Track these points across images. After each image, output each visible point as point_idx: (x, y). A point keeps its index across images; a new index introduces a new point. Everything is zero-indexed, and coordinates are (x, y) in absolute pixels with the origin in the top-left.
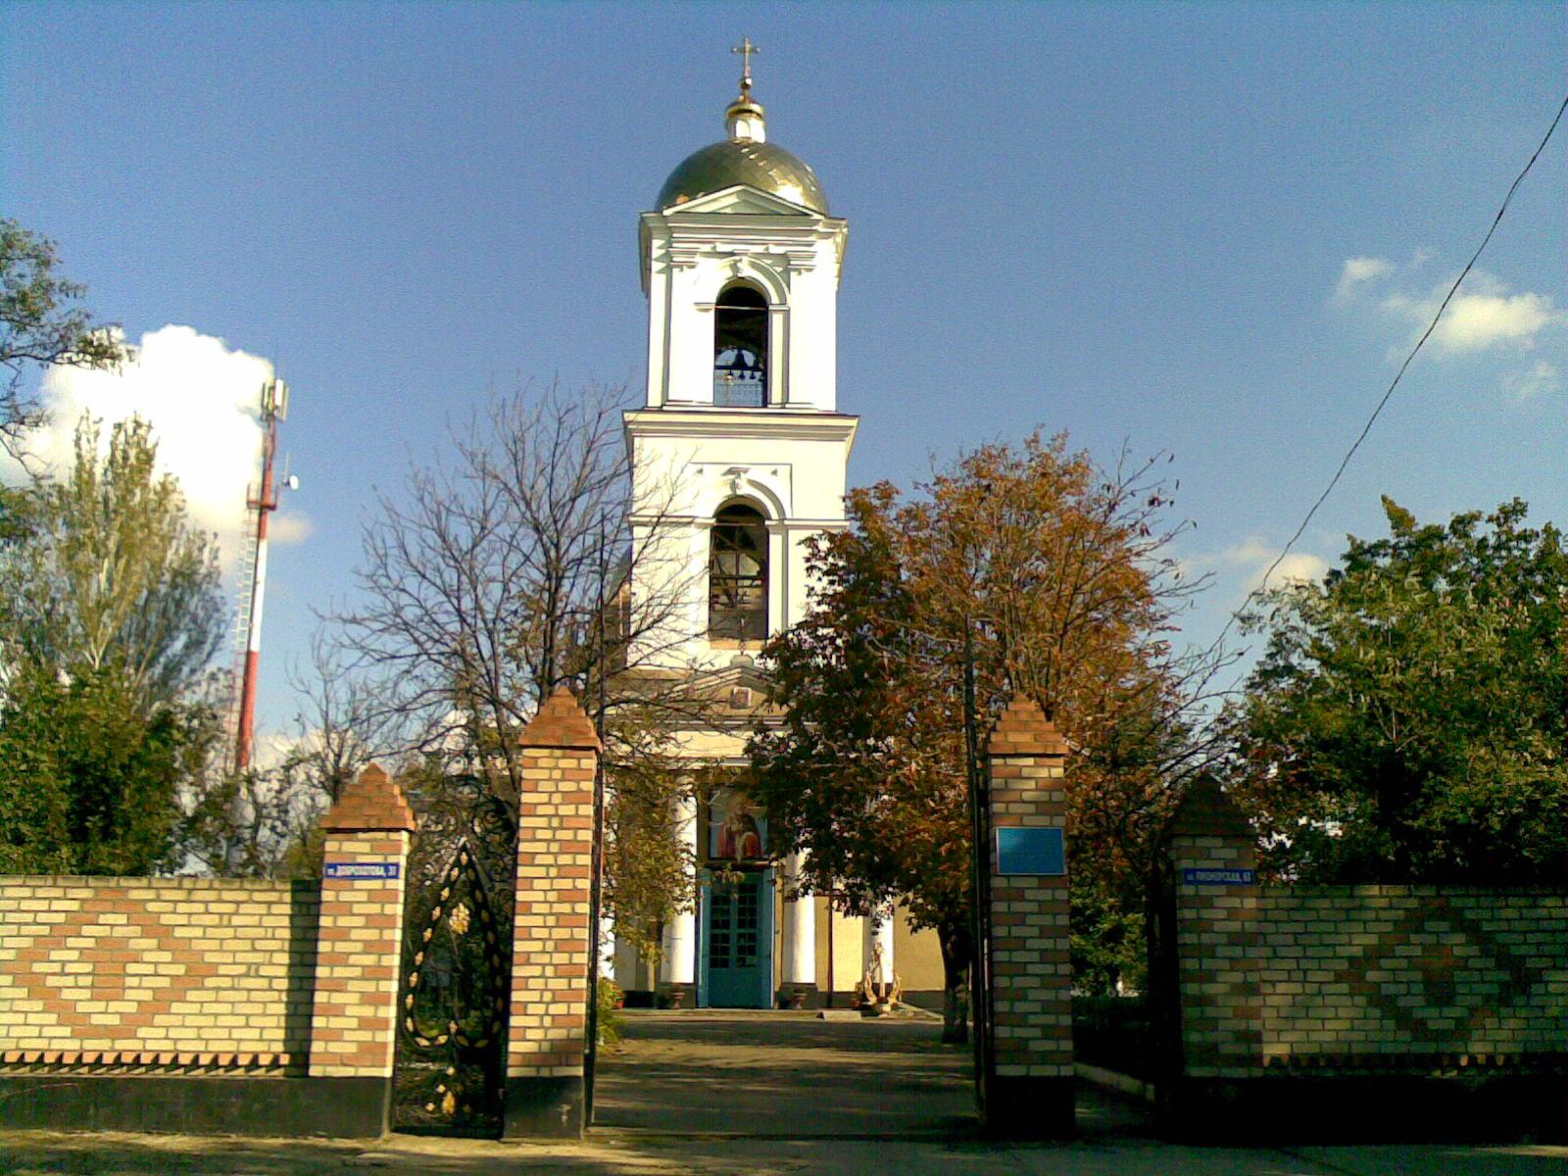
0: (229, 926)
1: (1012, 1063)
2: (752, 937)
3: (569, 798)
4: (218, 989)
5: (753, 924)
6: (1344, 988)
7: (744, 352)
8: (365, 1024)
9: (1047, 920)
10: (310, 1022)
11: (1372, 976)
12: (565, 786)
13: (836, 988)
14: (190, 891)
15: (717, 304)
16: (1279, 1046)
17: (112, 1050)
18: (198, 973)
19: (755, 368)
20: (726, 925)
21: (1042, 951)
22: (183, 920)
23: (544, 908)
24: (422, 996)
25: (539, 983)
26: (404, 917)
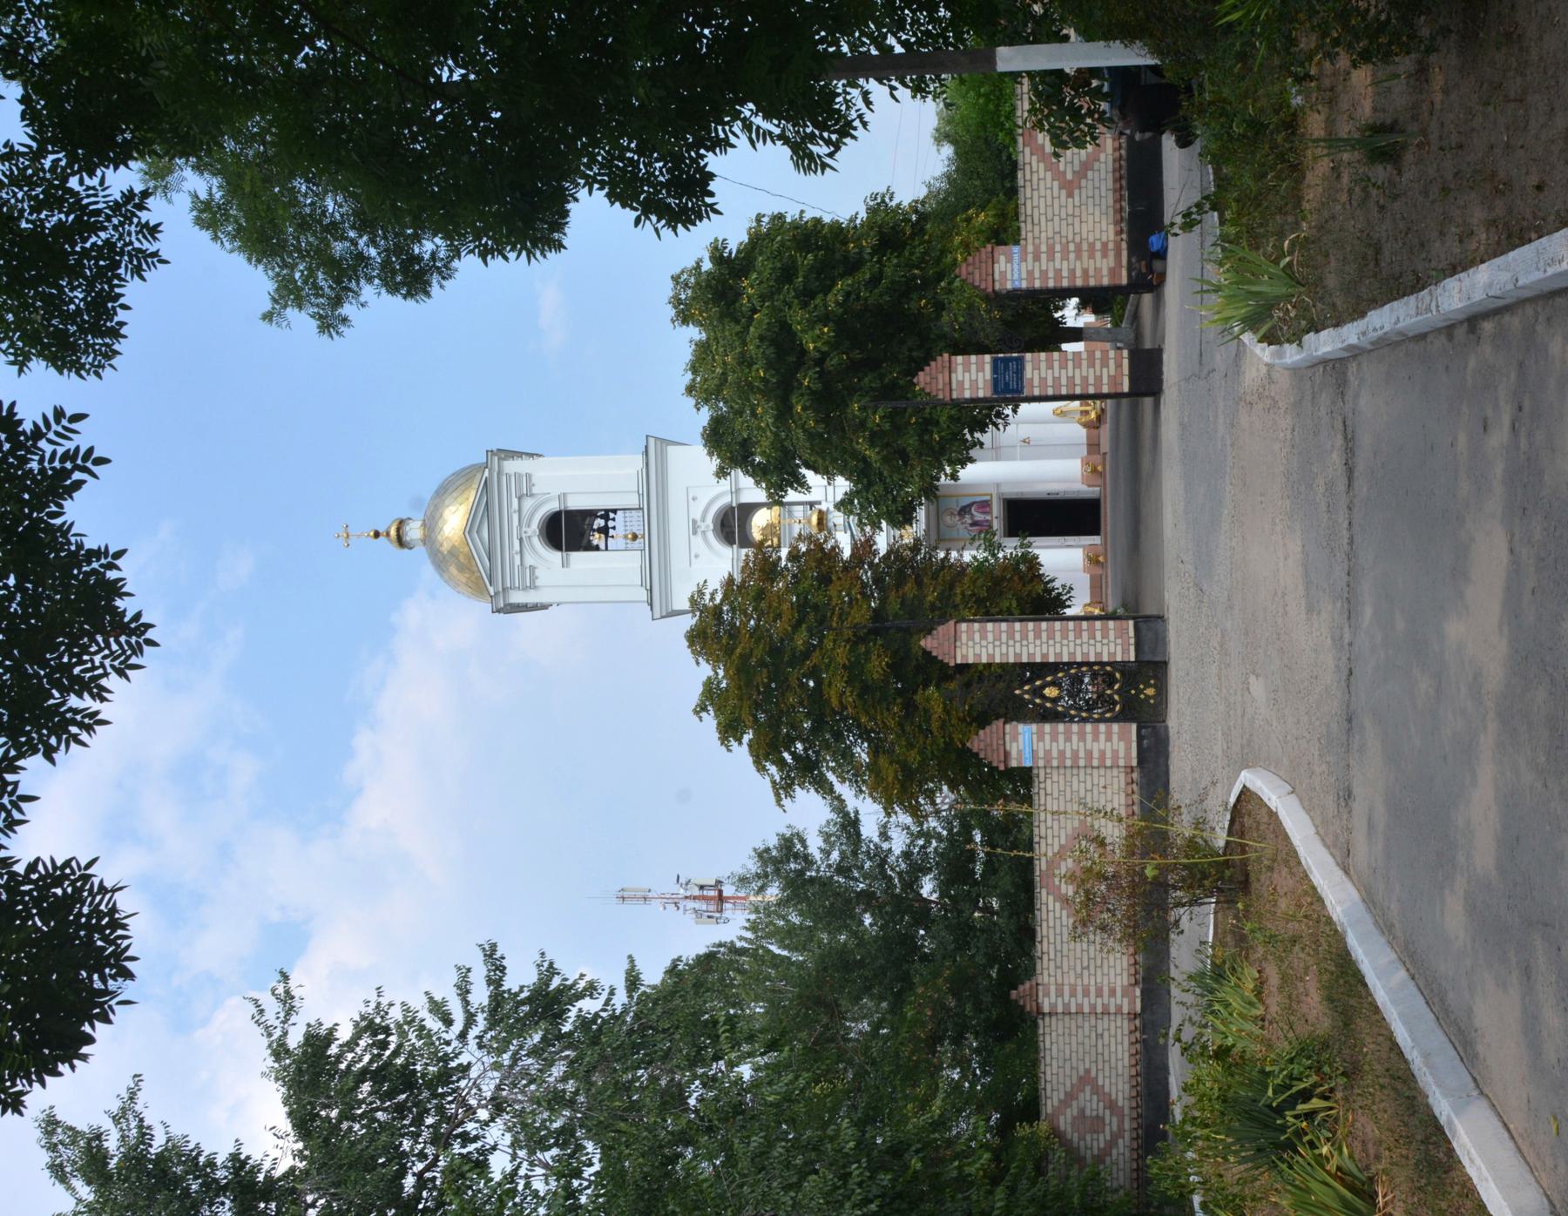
6: (1076, 192)
11: (1069, 176)
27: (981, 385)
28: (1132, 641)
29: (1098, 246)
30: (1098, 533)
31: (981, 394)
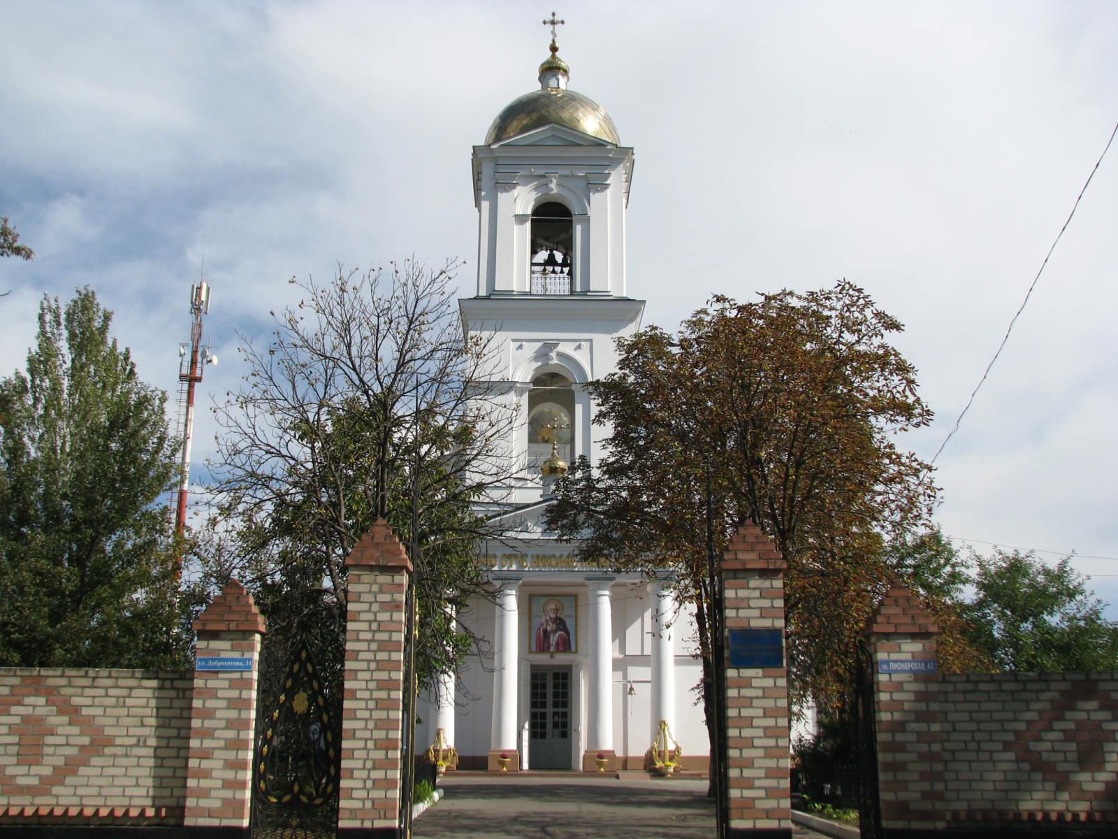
0: (124, 706)
1: (742, 818)
2: (565, 715)
3: (385, 607)
4: (115, 756)
5: (565, 704)
7: (555, 252)
8: (227, 784)
9: (769, 703)
10: (186, 783)
12: (381, 598)
13: (631, 754)
14: (94, 678)
15: (533, 215)
16: (1032, 802)
17: (32, 804)
18: (99, 743)
19: (564, 264)
20: (544, 705)
21: (766, 728)
22: (89, 701)
23: (366, 695)
24: (270, 762)
25: (363, 754)
26: (258, 700)
27: (742, 613)
28: (367, 824)
29: (939, 786)
30: (531, 767)
31: (729, 613)
